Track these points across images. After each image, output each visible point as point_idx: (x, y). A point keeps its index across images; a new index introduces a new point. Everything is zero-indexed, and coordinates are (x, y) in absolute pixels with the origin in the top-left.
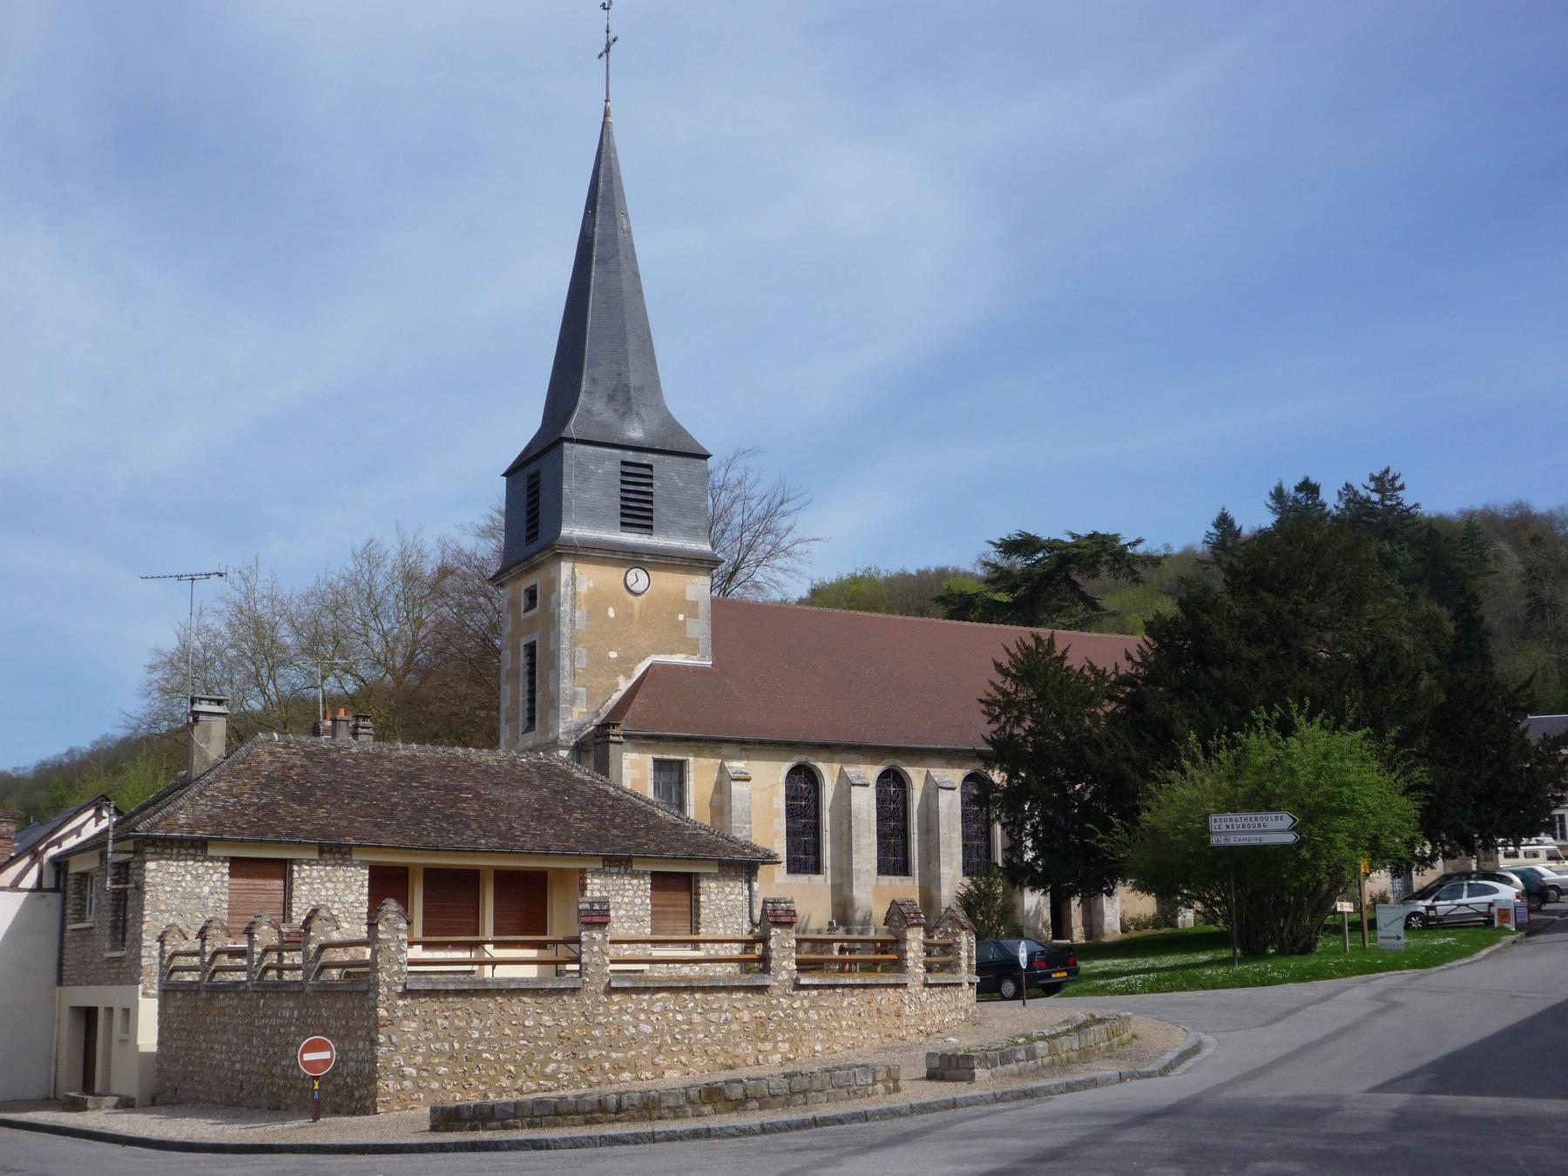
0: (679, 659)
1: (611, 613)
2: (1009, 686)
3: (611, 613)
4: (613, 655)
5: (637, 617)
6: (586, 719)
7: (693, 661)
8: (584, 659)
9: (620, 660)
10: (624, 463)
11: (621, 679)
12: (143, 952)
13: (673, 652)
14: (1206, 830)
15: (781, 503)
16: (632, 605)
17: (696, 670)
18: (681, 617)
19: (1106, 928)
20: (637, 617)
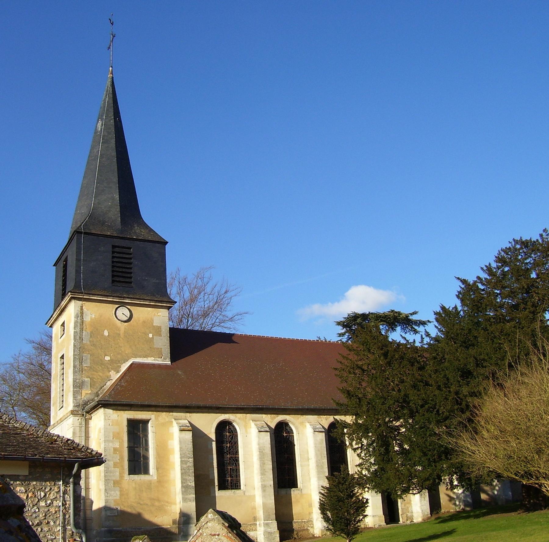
0: (150, 360)
1: (106, 333)
2: (353, 357)
3: (106, 333)
4: (107, 358)
5: (122, 336)
6: (92, 397)
7: (159, 361)
8: (89, 361)
9: (111, 361)
10: (114, 247)
11: (112, 373)
12: (48, 483)
13: (146, 356)
14: (387, 337)
15: (226, 292)
16: (119, 330)
17: (160, 366)
18: (151, 336)
19: (295, 526)
20: (122, 336)
